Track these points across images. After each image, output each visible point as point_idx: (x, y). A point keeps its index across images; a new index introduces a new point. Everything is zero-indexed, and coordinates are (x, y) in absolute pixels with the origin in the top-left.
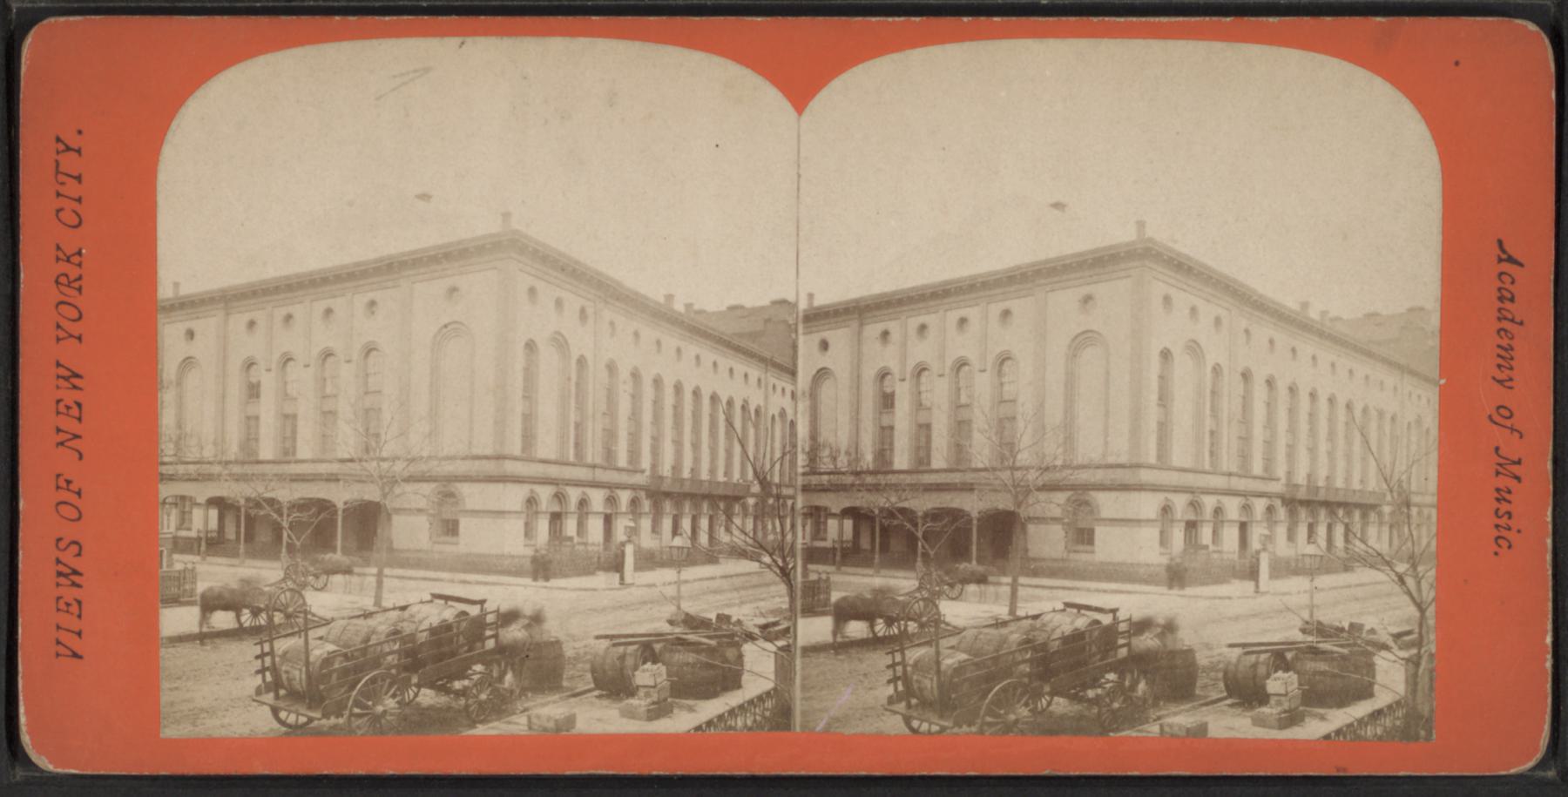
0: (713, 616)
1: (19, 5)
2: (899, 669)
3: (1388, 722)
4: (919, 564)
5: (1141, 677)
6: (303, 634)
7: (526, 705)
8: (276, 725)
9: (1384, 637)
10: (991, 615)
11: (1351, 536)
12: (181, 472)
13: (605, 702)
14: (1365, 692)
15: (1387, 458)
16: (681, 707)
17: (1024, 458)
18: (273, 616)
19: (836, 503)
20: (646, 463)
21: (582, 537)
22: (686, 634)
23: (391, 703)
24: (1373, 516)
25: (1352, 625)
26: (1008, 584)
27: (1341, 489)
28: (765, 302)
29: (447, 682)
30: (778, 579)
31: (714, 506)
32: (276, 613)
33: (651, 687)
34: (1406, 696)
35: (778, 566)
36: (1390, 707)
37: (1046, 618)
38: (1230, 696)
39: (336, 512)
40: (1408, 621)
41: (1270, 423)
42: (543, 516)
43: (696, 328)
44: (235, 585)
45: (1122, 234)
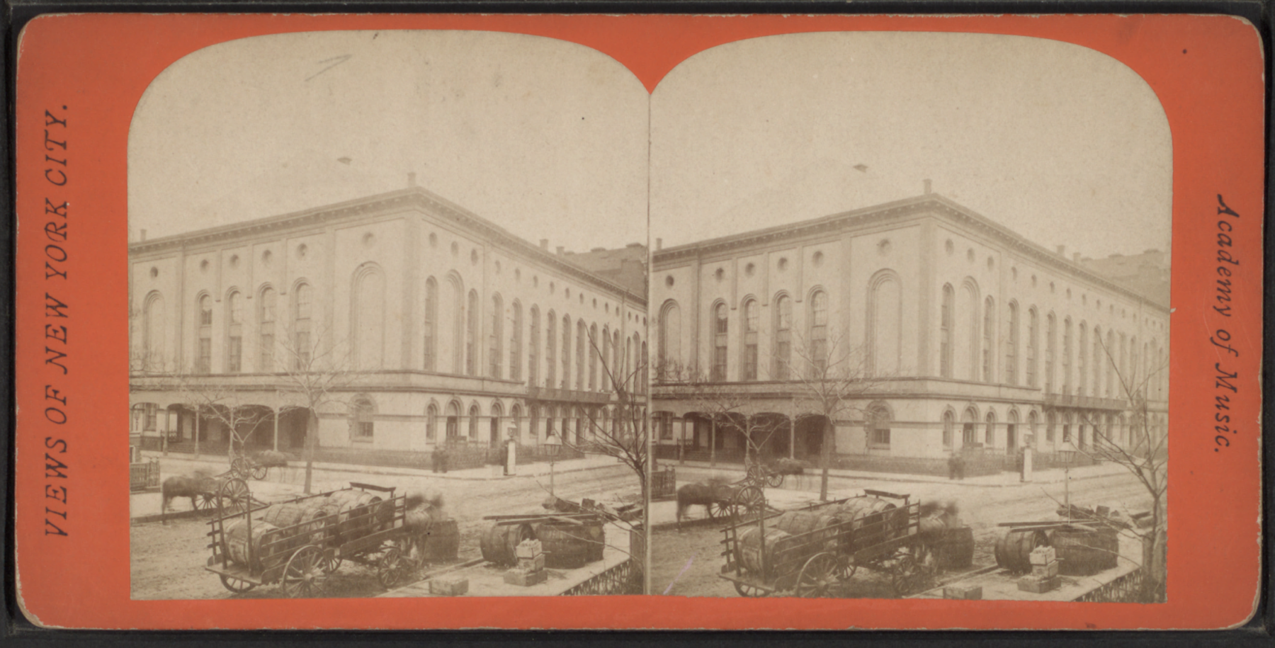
0: (580, 501)
1: (15, 4)
2: (731, 544)
3: (1129, 587)
4: (747, 458)
5: (928, 551)
6: (246, 515)
7: (428, 573)
8: (224, 589)
9: (1125, 518)
10: (806, 500)
11: (1098, 435)
12: (662, 392)
13: (492, 571)
14: (1110, 563)
15: (1128, 373)
16: (554, 575)
17: (832, 372)
18: (222, 501)
19: (679, 409)
20: (525, 377)
22: (558, 515)
23: (318, 572)
24: (1116, 420)
25: (1099, 508)
27: (1091, 398)
28: (623, 245)
29: (364, 555)
30: (632, 471)
31: (580, 412)
32: (224, 499)
33: (1042, 565)
35: (633, 460)
36: (1130, 575)
37: (851, 503)
38: (1000, 566)
40: (1145, 505)
41: (1033, 344)
42: (441, 419)
43: (566, 267)
44: (191, 476)
45: (912, 190)
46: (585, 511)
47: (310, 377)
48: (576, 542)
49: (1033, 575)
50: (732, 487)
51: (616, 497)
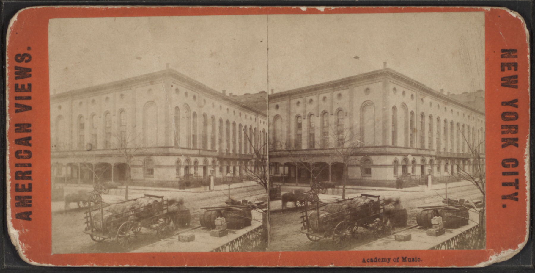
0: (241, 201)
1: (5, 2)
2: (305, 218)
3: (473, 233)
4: (311, 182)
5: (388, 219)
7: (178, 232)
8: (308, 240)
11: (459, 169)
12: (274, 154)
13: (205, 231)
14: (465, 222)
15: (471, 142)
16: (231, 232)
17: (129, 145)
21: (396, 175)
22: (232, 207)
23: (131, 233)
24: (467, 162)
25: (460, 200)
26: (124, 189)
27: (456, 153)
29: (367, 224)
30: (263, 187)
31: (241, 163)
32: (91, 203)
33: (437, 224)
34: (480, 224)
35: (263, 183)
36: (474, 227)
37: (356, 199)
39: (111, 167)
40: (480, 198)
42: (400, 166)
43: (233, 101)
44: (77, 193)
45: (378, 66)
46: (243, 205)
47: (344, 150)
48: (240, 218)
49: (433, 229)
50: (305, 194)
51: (256, 199)
